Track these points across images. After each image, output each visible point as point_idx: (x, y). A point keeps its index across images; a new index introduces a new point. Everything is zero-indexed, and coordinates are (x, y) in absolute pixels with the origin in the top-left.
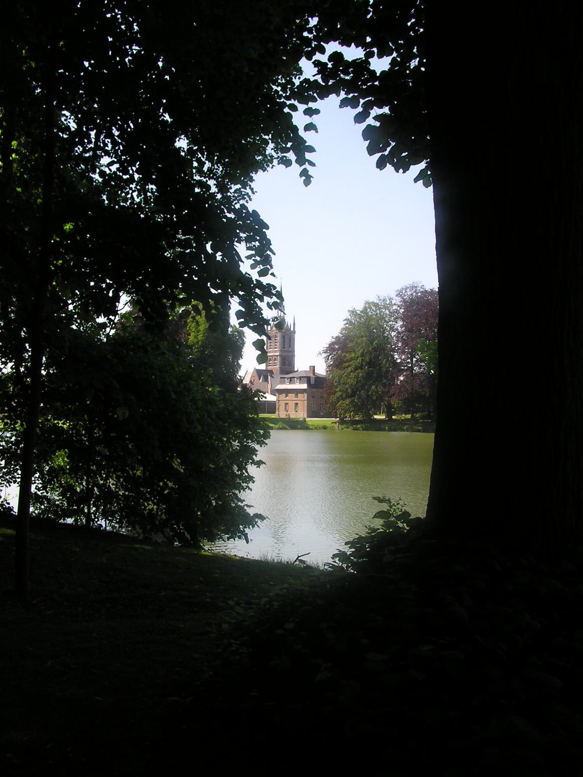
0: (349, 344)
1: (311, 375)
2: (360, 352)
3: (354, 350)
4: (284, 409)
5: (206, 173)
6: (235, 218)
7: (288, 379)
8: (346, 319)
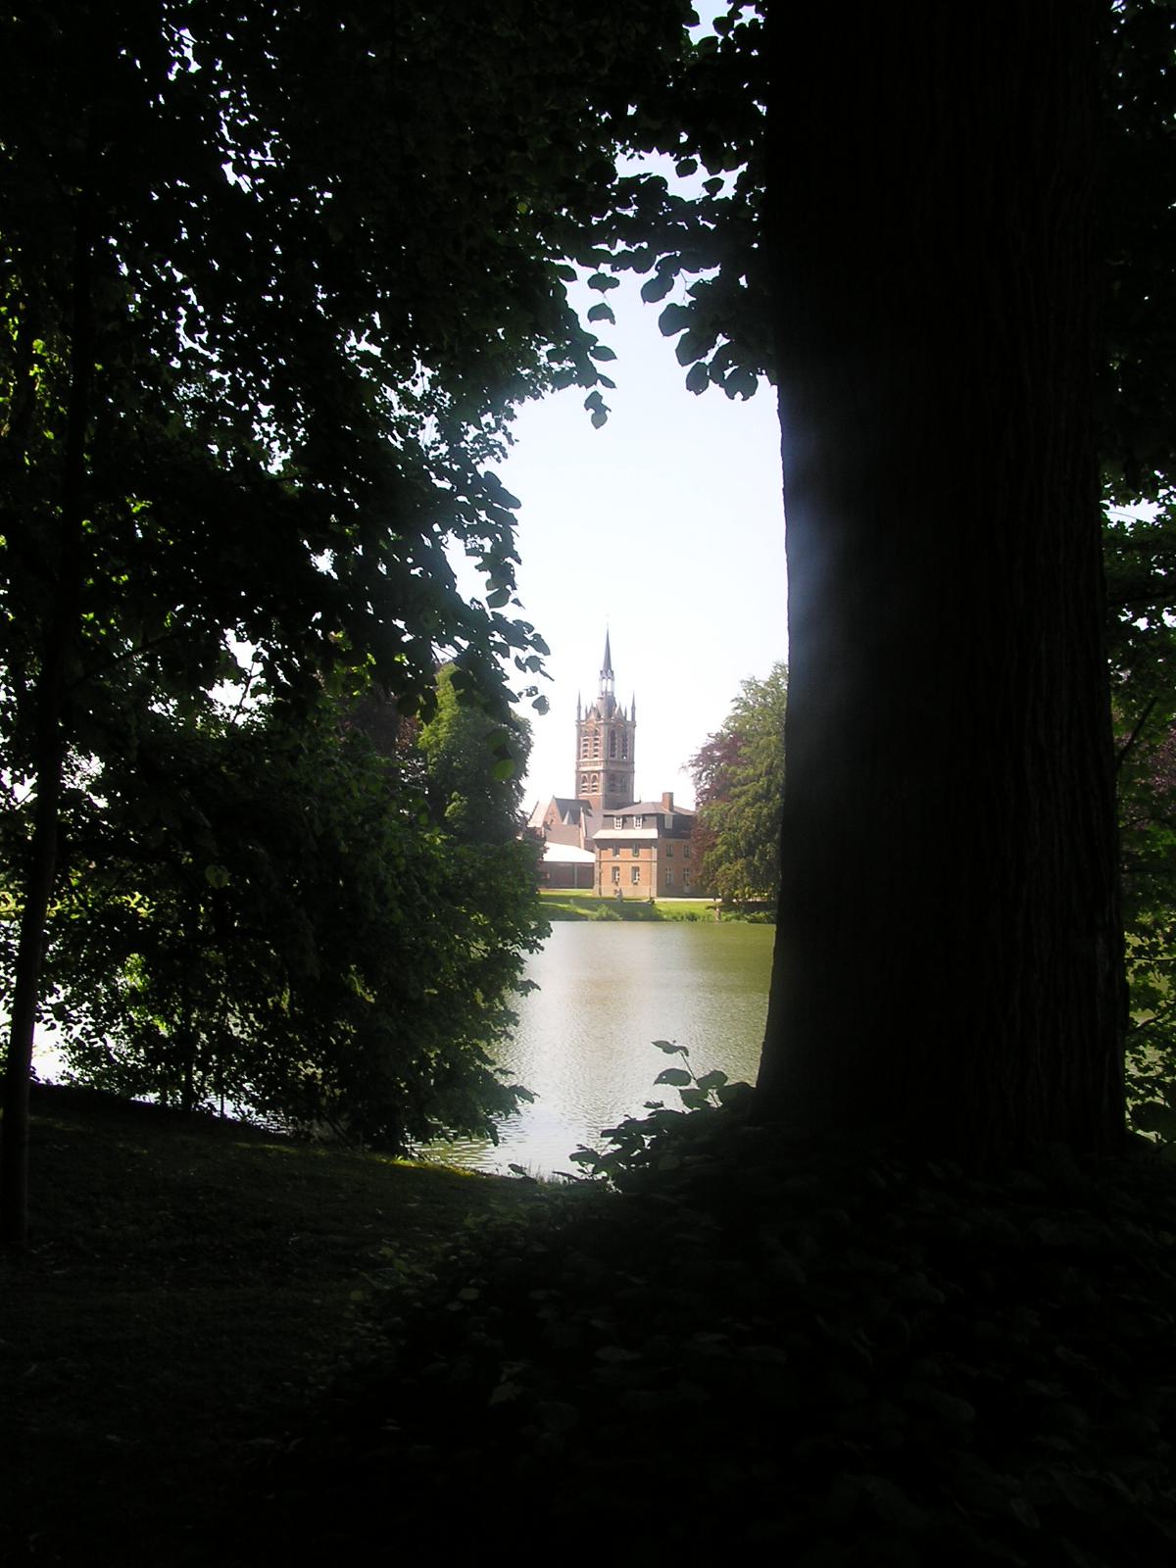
0: (743, 748)
1: (666, 811)
2: (765, 764)
3: (752, 761)
4: (610, 878)
5: (412, 403)
6: (452, 488)
7: (618, 818)
8: (736, 699)
